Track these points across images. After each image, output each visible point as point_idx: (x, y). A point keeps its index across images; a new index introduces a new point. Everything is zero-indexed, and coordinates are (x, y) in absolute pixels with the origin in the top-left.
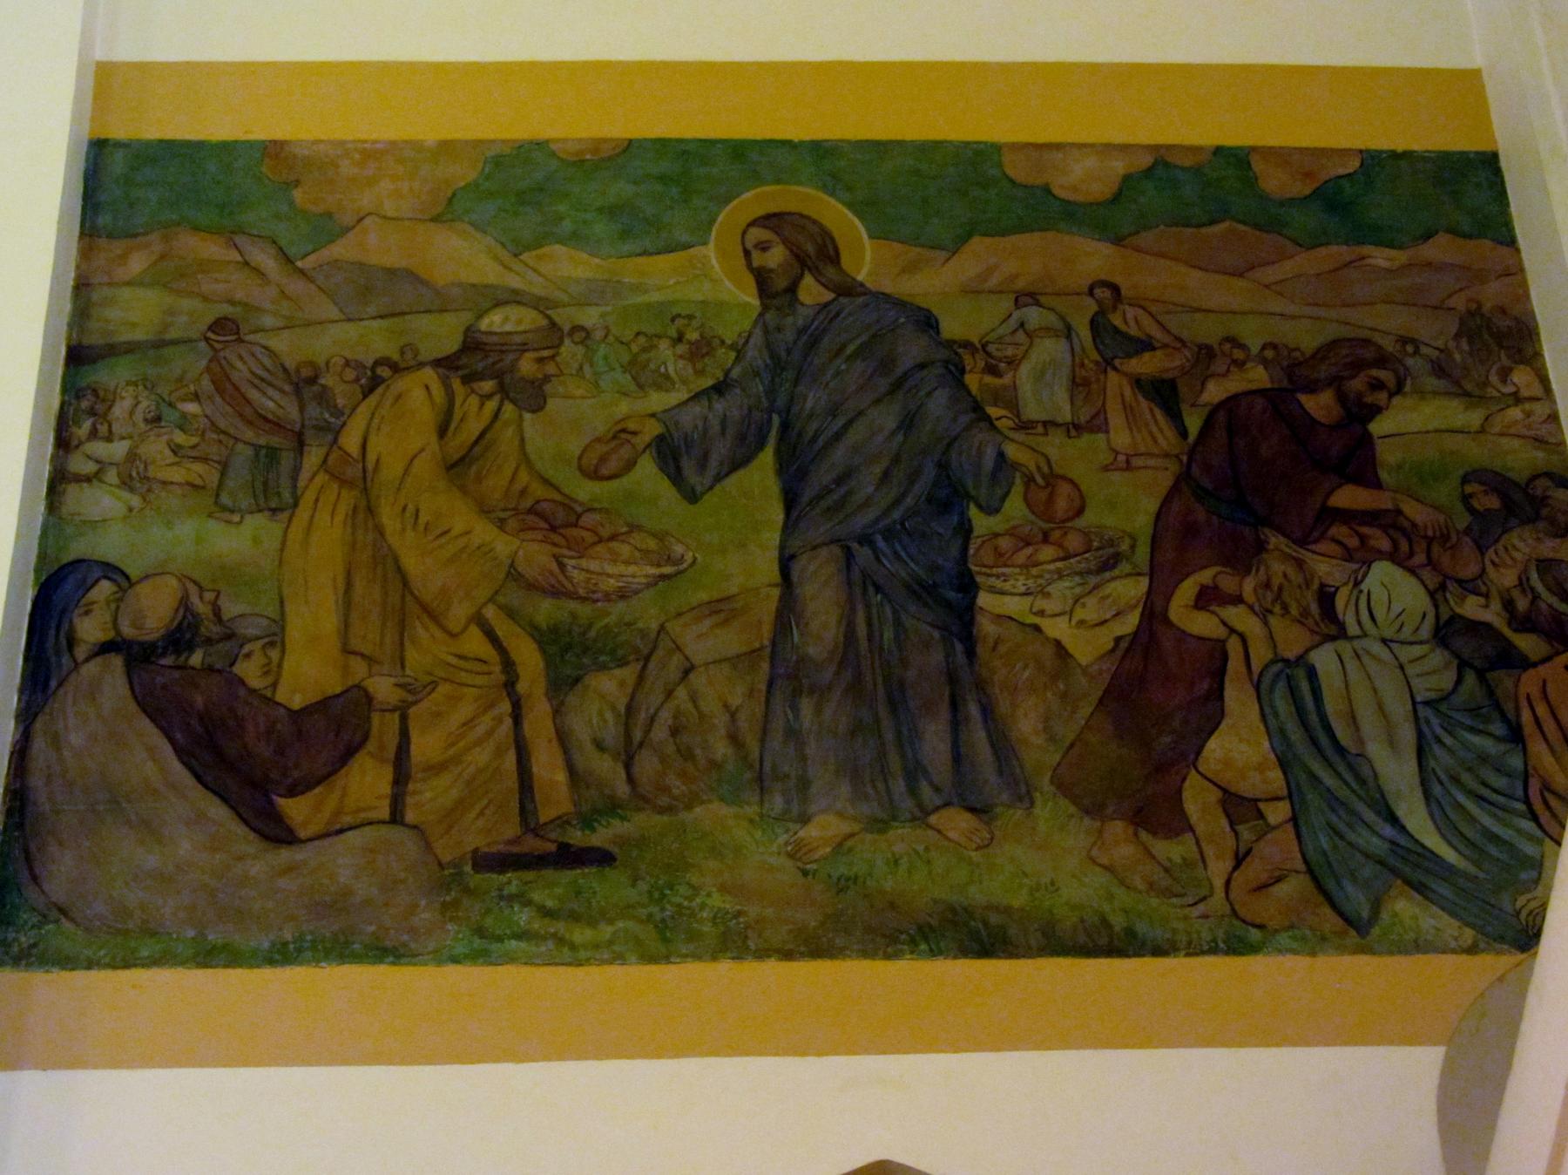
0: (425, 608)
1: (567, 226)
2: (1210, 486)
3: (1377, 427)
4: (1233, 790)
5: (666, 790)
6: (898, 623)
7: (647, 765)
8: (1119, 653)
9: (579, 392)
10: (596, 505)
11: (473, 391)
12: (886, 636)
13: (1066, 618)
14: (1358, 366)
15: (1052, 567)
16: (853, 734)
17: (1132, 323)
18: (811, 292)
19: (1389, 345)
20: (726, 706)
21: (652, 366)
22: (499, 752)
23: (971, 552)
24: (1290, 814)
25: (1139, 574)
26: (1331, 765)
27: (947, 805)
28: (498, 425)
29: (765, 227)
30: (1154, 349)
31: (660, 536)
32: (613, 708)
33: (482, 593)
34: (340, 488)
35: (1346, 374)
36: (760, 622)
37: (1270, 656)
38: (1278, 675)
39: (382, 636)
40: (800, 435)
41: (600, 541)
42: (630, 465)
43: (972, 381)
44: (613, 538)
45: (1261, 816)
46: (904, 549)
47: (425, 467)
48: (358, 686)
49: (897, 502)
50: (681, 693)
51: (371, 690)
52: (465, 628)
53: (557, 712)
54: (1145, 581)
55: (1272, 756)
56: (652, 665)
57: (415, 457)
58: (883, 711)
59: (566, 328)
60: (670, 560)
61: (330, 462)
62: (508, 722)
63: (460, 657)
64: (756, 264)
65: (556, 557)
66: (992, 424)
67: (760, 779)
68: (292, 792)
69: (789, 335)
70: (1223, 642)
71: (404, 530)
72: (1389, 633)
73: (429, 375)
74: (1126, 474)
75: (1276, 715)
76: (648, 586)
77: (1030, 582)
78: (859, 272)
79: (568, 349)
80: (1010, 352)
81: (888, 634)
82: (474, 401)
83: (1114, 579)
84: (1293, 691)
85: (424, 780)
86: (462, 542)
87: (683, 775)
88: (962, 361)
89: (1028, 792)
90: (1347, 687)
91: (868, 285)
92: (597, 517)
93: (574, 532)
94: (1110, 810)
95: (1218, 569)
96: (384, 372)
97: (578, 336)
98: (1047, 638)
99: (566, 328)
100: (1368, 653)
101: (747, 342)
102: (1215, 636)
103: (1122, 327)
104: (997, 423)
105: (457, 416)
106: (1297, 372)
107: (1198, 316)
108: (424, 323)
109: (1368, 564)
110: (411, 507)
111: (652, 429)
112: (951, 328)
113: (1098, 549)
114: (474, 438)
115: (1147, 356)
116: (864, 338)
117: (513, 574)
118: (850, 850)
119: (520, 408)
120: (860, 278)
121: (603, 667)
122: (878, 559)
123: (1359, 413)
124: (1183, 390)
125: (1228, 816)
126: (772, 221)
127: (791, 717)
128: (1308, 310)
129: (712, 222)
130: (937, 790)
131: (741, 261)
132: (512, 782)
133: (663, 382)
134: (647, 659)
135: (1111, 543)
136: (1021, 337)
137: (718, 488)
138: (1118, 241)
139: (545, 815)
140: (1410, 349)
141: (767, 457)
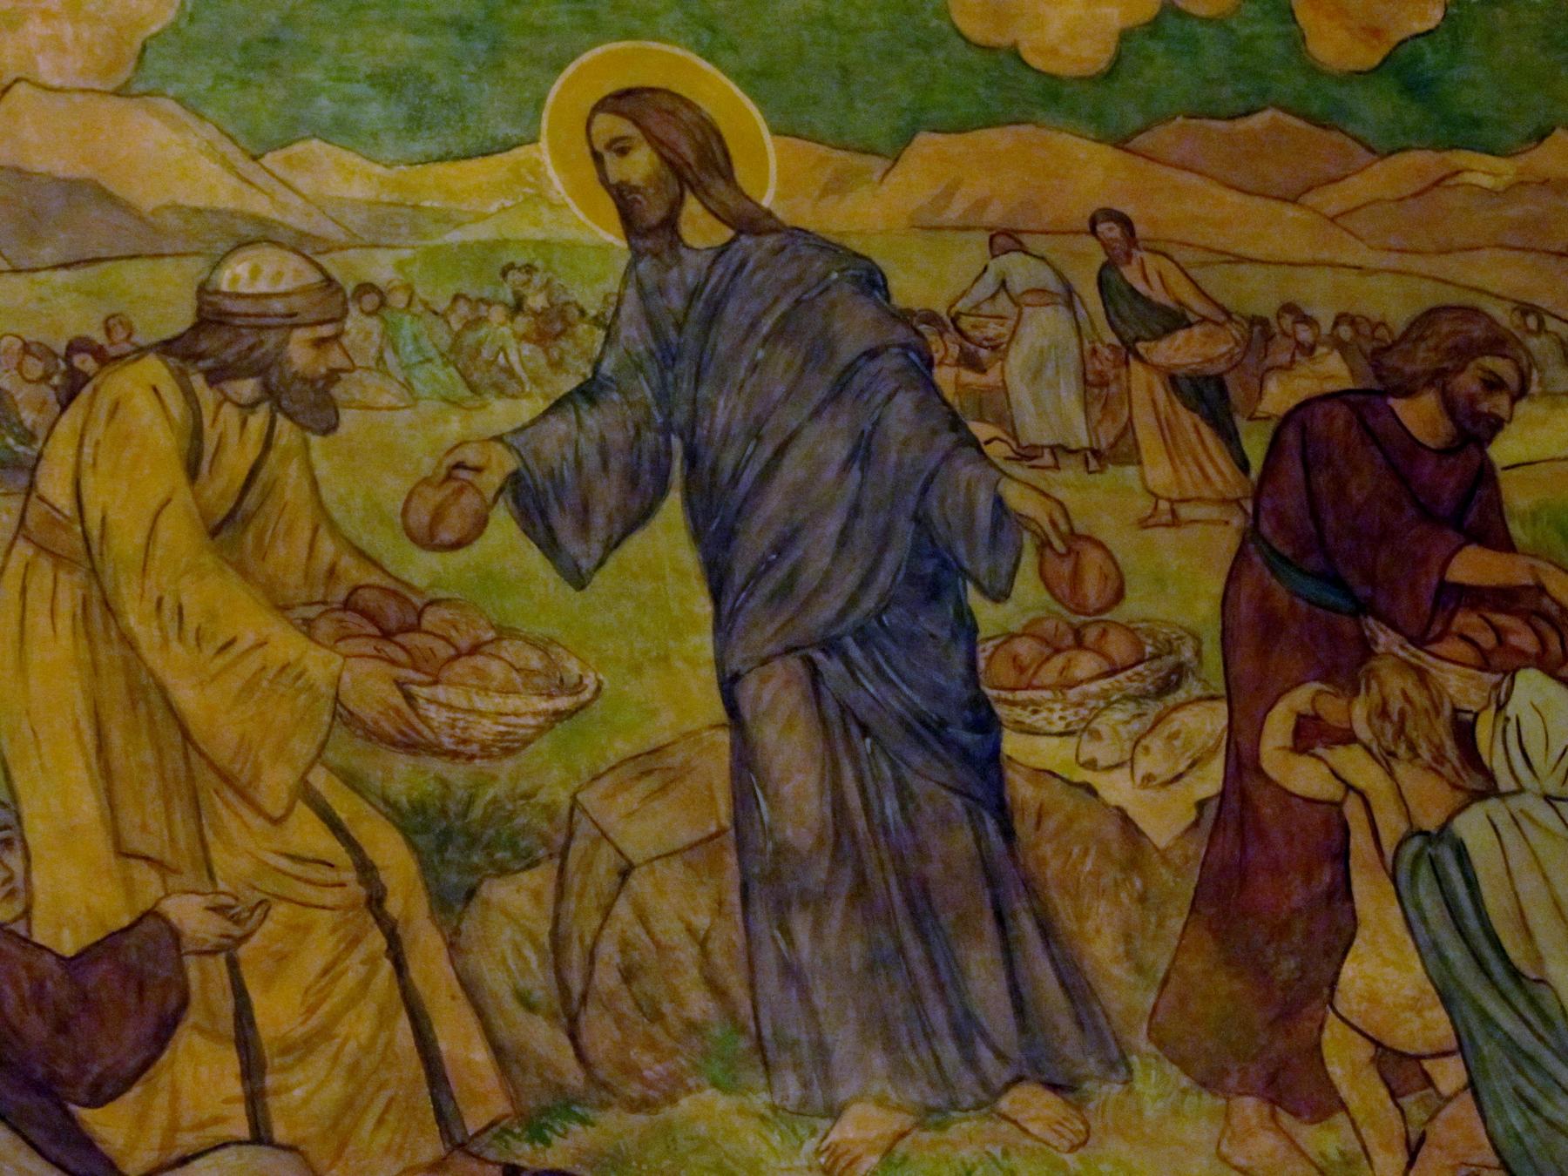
0: (227, 778)
1: (325, 106)
2: (1287, 551)
3: (1503, 450)
4: (1388, 1043)
5: (630, 1070)
6: (902, 789)
7: (600, 1032)
8: (1207, 824)
9: (385, 400)
10: (442, 594)
11: (226, 399)
12: (888, 811)
13: (1127, 770)
14: (1465, 352)
15: (1094, 687)
16: (871, 968)
17: (1154, 279)
18: (700, 228)
19: (1501, 314)
20: (690, 930)
21: (486, 354)
22: (384, 1020)
23: (982, 664)
24: (1464, 1077)
25: (1213, 698)
26: (1510, 1004)
27: (1018, 1080)
28: (273, 456)
29: (618, 113)
30: (1190, 325)
31: (543, 646)
32: (533, 938)
33: (303, 747)
34: (56, 567)
35: (1448, 364)
36: (710, 787)
37: (1403, 827)
38: (1417, 858)
39: (169, 818)
40: (714, 470)
41: (459, 655)
42: (481, 524)
43: (944, 376)
44: (475, 650)
45: (1428, 1081)
46: (888, 660)
47: (179, 532)
48: (152, 913)
49: (865, 584)
50: (623, 909)
51: (173, 917)
52: (290, 810)
53: (453, 947)
54: (1223, 707)
55: (1429, 987)
56: (572, 863)
57: (158, 514)
58: (908, 936)
59: (349, 288)
60: (563, 687)
61: (30, 523)
62: (387, 966)
63: (293, 858)
64: (614, 178)
65: (400, 685)
66: (981, 451)
67: (760, 1046)
68: (99, 1097)
69: (677, 301)
70: (1338, 805)
71: (166, 641)
72: (1552, 787)
73: (154, 369)
74: (1172, 530)
75: (1424, 920)
76: (540, 730)
77: (1069, 713)
78: (763, 189)
79: (357, 324)
80: (992, 329)
81: (891, 806)
82: (229, 414)
83: (1177, 708)
84: (1440, 879)
85: (284, 1069)
86: (254, 662)
87: (651, 1045)
88: (928, 347)
89: (1124, 1057)
90: (1509, 873)
91: (779, 214)
92: (447, 614)
93: (415, 640)
94: (1232, 1082)
95: (1317, 686)
96: (85, 362)
97: (370, 301)
98: (1106, 805)
99: (349, 288)
100: (1530, 818)
101: (617, 313)
102: (1326, 796)
103: (1141, 287)
104: (987, 449)
105: (209, 447)
106: (1386, 364)
107: (1243, 269)
108: (134, 275)
109: (1512, 673)
110: (169, 604)
111: (503, 463)
112: (908, 289)
113: (1154, 657)
114: (240, 481)
115: (1181, 335)
116: (783, 307)
117: (343, 715)
118: (905, 1158)
119: (304, 428)
120: (766, 202)
121: (503, 871)
122: (853, 674)
123: (1474, 429)
124: (1236, 394)
125: (1388, 1085)
126: (623, 101)
127: (782, 945)
128: (1394, 261)
129: (539, 104)
130: (1000, 1056)
131: (590, 170)
132: (413, 1066)
133: (505, 383)
134: (564, 854)
135: (1169, 647)
136: (1003, 304)
137: (612, 562)
138: (1122, 143)
139: (474, 1121)
140: (1532, 322)
141: (673, 506)
